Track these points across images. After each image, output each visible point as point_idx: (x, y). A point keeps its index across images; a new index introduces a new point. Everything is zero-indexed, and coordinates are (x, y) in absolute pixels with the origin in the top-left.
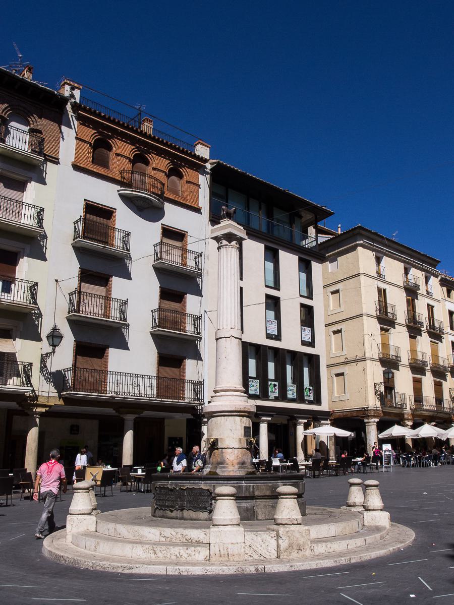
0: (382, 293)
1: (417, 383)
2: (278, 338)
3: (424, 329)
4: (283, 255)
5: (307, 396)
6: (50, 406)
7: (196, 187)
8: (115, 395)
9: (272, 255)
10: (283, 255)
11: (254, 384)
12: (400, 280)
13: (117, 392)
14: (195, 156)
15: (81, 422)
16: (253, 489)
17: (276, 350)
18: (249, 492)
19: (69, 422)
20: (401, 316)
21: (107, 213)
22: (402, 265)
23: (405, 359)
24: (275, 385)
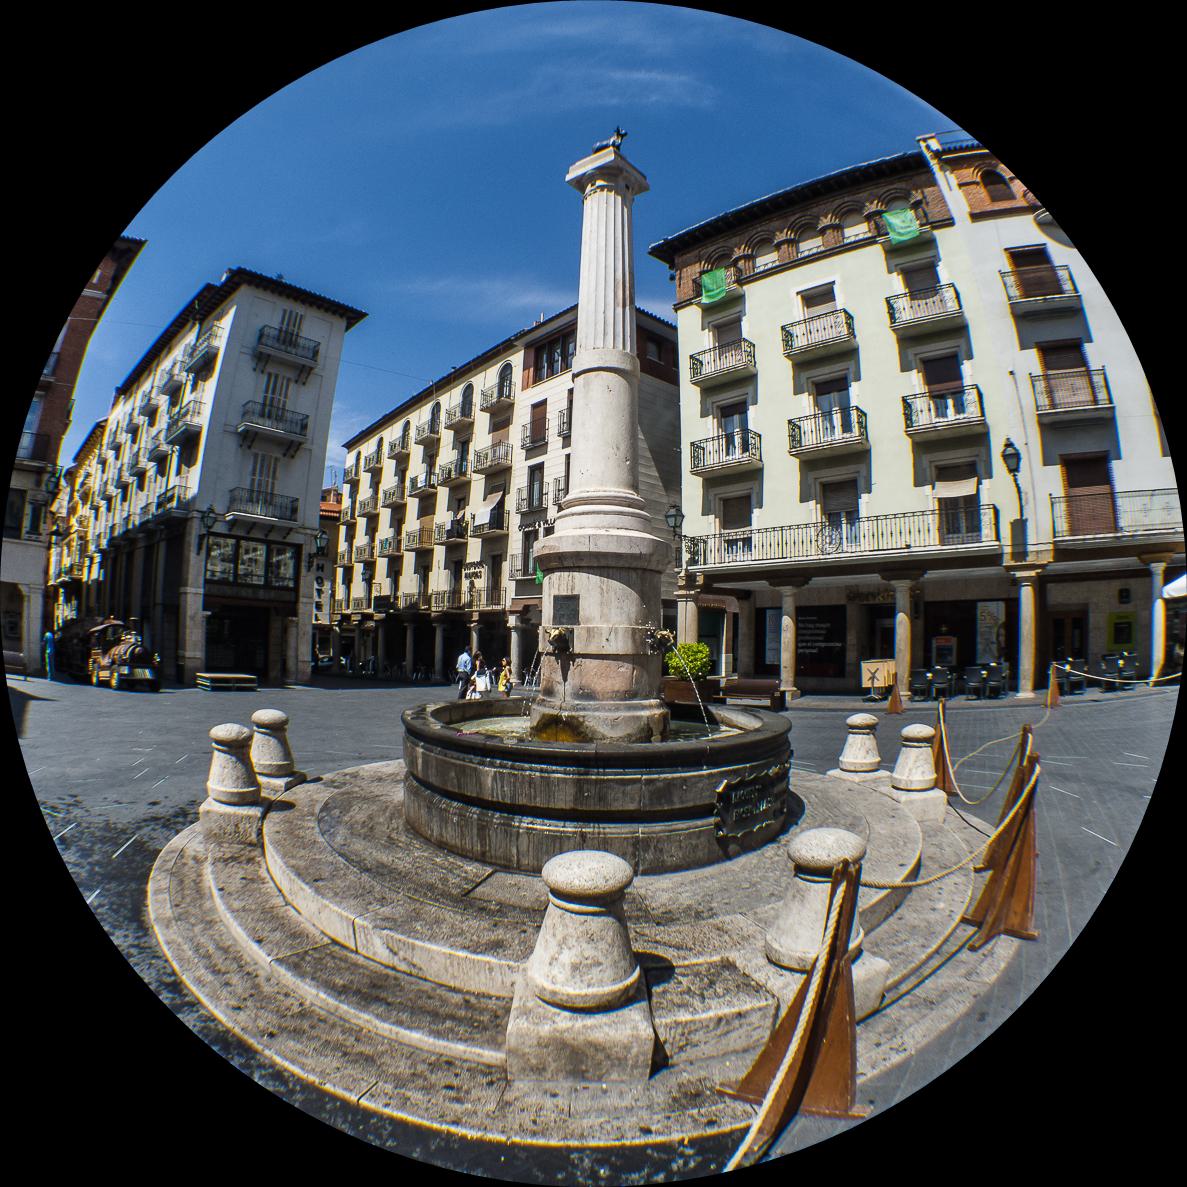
6: (1042, 566)
19: (1116, 585)
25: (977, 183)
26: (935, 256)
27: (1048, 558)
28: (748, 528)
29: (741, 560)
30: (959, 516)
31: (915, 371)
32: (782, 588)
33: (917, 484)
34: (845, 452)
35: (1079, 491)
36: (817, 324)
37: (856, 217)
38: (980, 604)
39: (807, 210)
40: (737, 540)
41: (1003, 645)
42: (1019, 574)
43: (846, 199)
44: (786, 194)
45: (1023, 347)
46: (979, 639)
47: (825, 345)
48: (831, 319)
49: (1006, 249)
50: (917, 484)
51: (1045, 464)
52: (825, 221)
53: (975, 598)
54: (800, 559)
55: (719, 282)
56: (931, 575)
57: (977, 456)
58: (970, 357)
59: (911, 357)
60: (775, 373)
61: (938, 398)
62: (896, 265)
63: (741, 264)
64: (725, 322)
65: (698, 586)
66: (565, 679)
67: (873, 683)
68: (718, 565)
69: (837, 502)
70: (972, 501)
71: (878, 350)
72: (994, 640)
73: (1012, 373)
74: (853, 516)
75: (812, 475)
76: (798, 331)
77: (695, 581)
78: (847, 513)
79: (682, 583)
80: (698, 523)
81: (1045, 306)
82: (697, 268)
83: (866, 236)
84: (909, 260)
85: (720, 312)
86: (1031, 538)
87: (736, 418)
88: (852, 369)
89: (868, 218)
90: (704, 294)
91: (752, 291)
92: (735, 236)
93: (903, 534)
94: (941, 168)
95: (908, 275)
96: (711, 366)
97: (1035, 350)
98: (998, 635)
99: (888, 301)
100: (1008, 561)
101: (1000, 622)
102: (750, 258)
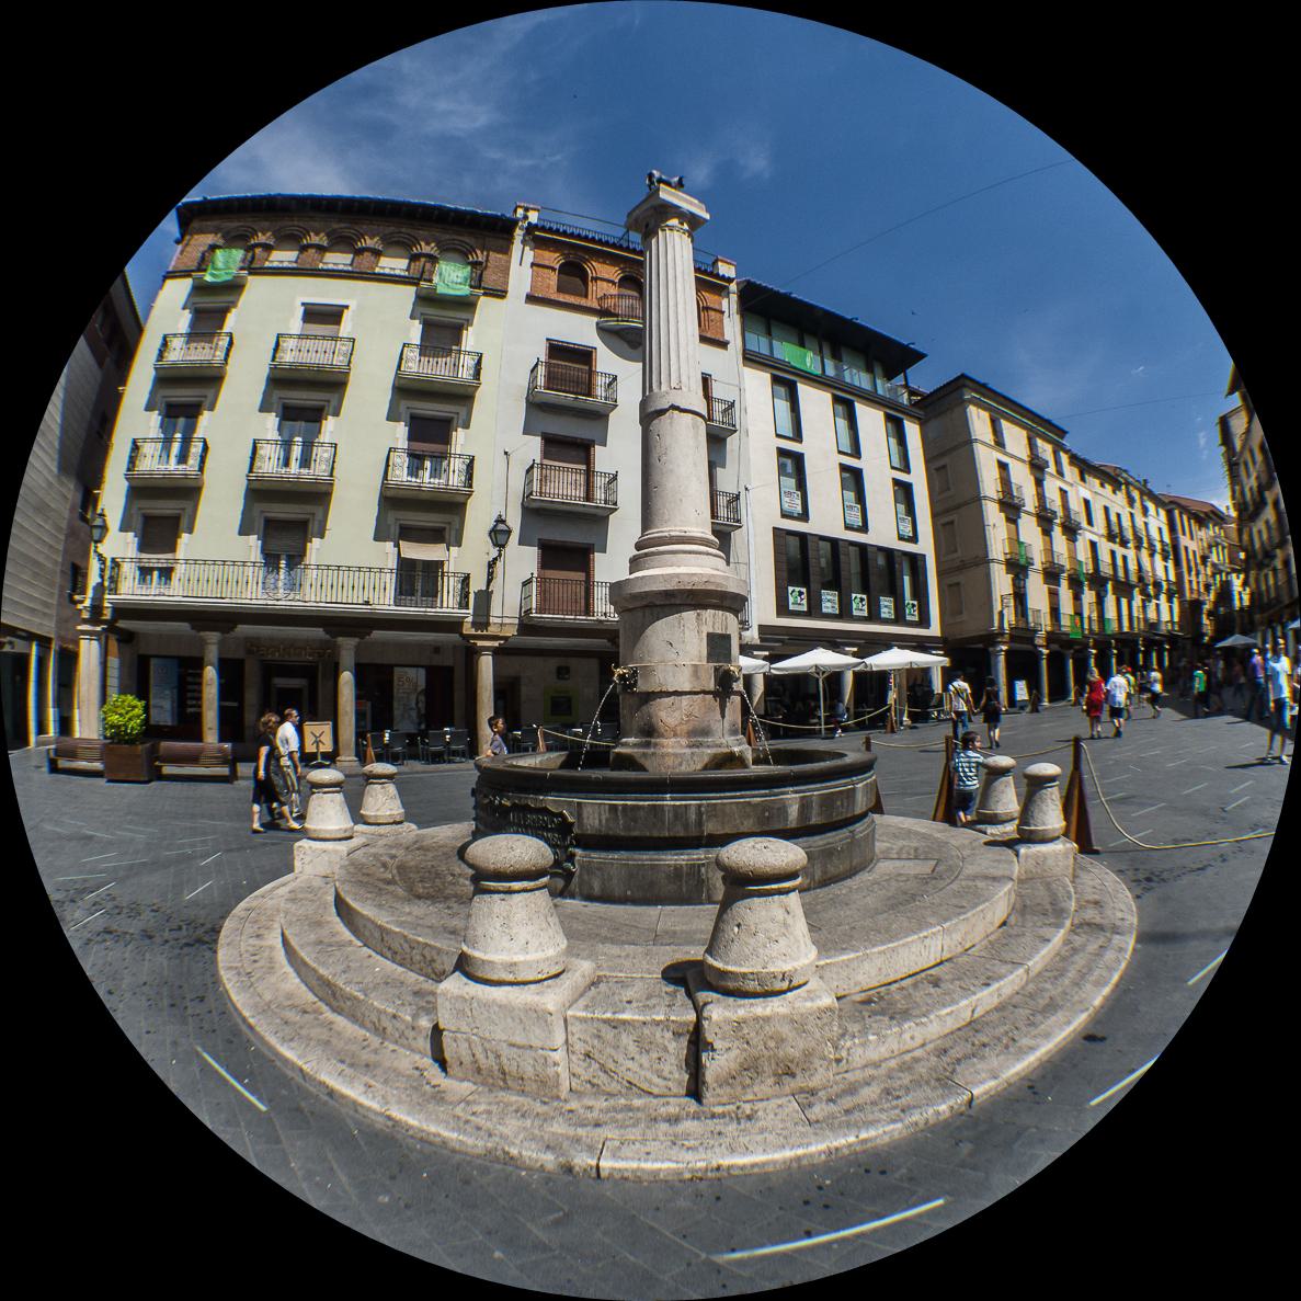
0: (1003, 466)
1: (1054, 595)
2: (864, 528)
3: (1058, 521)
4: (863, 411)
5: (910, 614)
6: (506, 638)
7: (718, 315)
8: (603, 618)
9: (844, 408)
10: (863, 411)
11: (886, 603)
12: (1024, 453)
13: (605, 614)
14: (717, 276)
15: (573, 662)
16: (699, 814)
17: (863, 548)
18: (686, 826)
19: (553, 663)
20: (1030, 504)
21: (585, 356)
22: (1024, 433)
23: (1038, 565)
24: (862, 600)
25: (553, 269)
26: (468, 320)
27: (511, 632)
28: (169, 556)
29: (153, 593)
30: (417, 579)
31: (403, 423)
32: (208, 633)
33: (377, 538)
34: (167, 484)
35: (550, 574)
36: (308, 344)
37: (401, 251)
38: (396, 668)
39: (356, 223)
40: (153, 569)
41: (423, 711)
42: (480, 643)
43: (403, 230)
44: (456, 211)
45: (526, 432)
46: (395, 704)
47: (309, 368)
48: (328, 345)
49: (548, 339)
50: (377, 538)
51: (519, 544)
52: (368, 241)
53: (393, 662)
54: (244, 601)
55: (227, 262)
56: (377, 634)
57: (449, 523)
58: (466, 426)
59: (275, 398)
60: (245, 381)
61: (416, 459)
62: (422, 314)
63: (258, 251)
64: (209, 312)
65: (105, 622)
66: (723, 717)
67: (318, 747)
68: (254, 602)
69: (283, 542)
70: (433, 569)
71: (369, 392)
72: (414, 705)
73: (506, 453)
74: (296, 558)
75: (258, 507)
76: (289, 344)
77: (101, 614)
78: (287, 556)
79: (86, 615)
80: (119, 544)
81: (576, 404)
82: (209, 239)
83: (346, 268)
84: (435, 313)
85: (209, 295)
86: (495, 610)
87: (181, 421)
88: (334, 403)
89: (414, 258)
90: (209, 271)
91: (256, 286)
92: (266, 220)
93: (240, 584)
94: (524, 242)
95: (428, 326)
96: (177, 354)
97: (539, 438)
98: (417, 703)
99: (279, 336)
100: (468, 629)
101: (419, 689)
102: (268, 248)
